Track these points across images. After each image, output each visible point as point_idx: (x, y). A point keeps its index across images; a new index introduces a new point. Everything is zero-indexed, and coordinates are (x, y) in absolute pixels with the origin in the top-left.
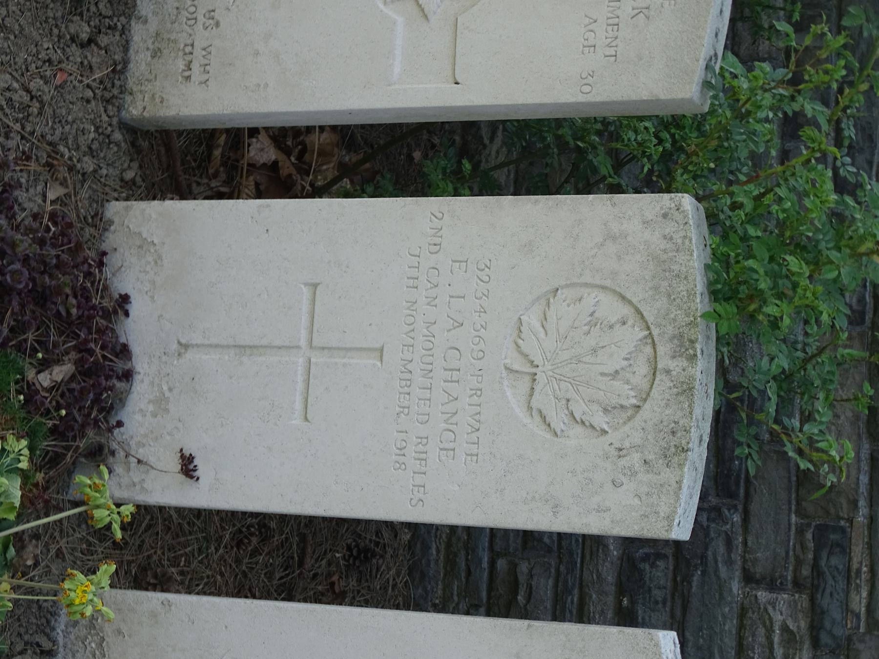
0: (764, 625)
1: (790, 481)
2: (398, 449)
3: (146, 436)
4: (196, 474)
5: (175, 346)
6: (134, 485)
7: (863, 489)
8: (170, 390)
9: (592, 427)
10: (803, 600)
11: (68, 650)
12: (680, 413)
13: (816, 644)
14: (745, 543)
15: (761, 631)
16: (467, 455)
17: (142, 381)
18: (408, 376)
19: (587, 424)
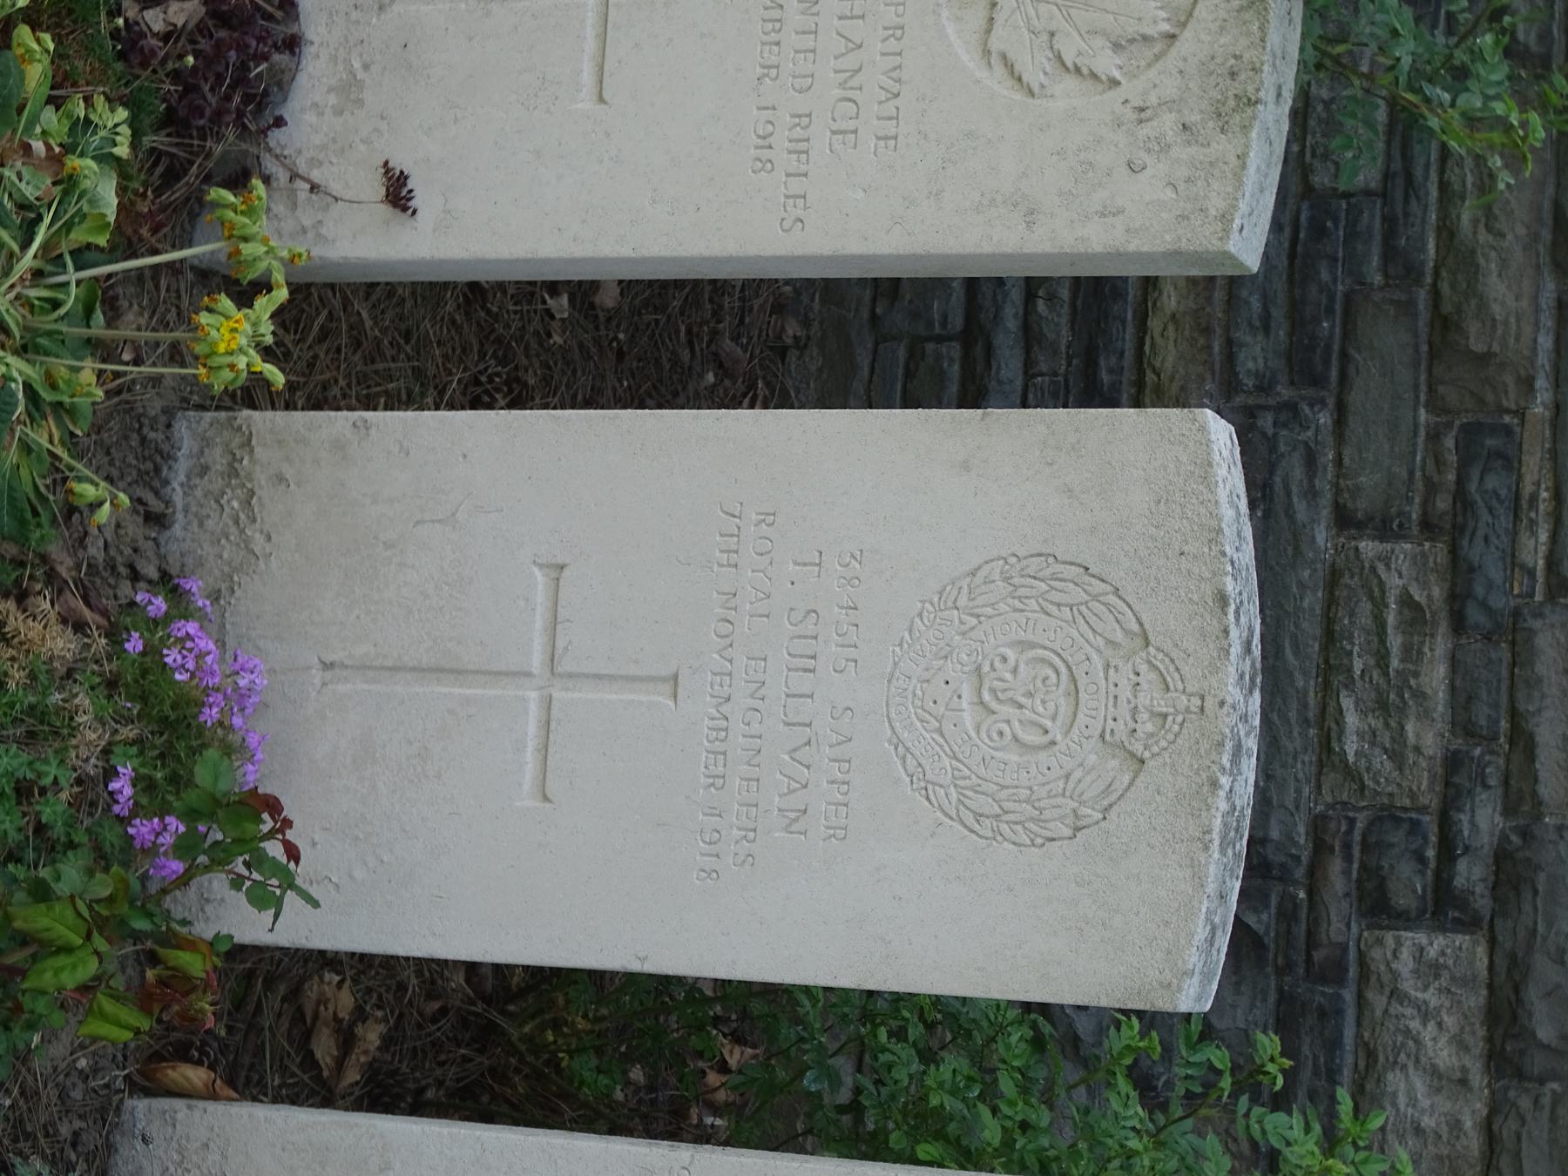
0: (1371, 598)
1: (1417, 351)
2: (759, 137)
3: (324, 147)
4: (412, 203)
6: (304, 231)
7: (1544, 359)
8: (366, 67)
9: (1094, 76)
10: (1438, 552)
11: (190, 516)
12: (1244, 42)
13: (1458, 624)
14: (1339, 462)
15: (1365, 607)
16: (878, 138)
17: (318, 56)
18: (776, 14)
19: (1085, 71)
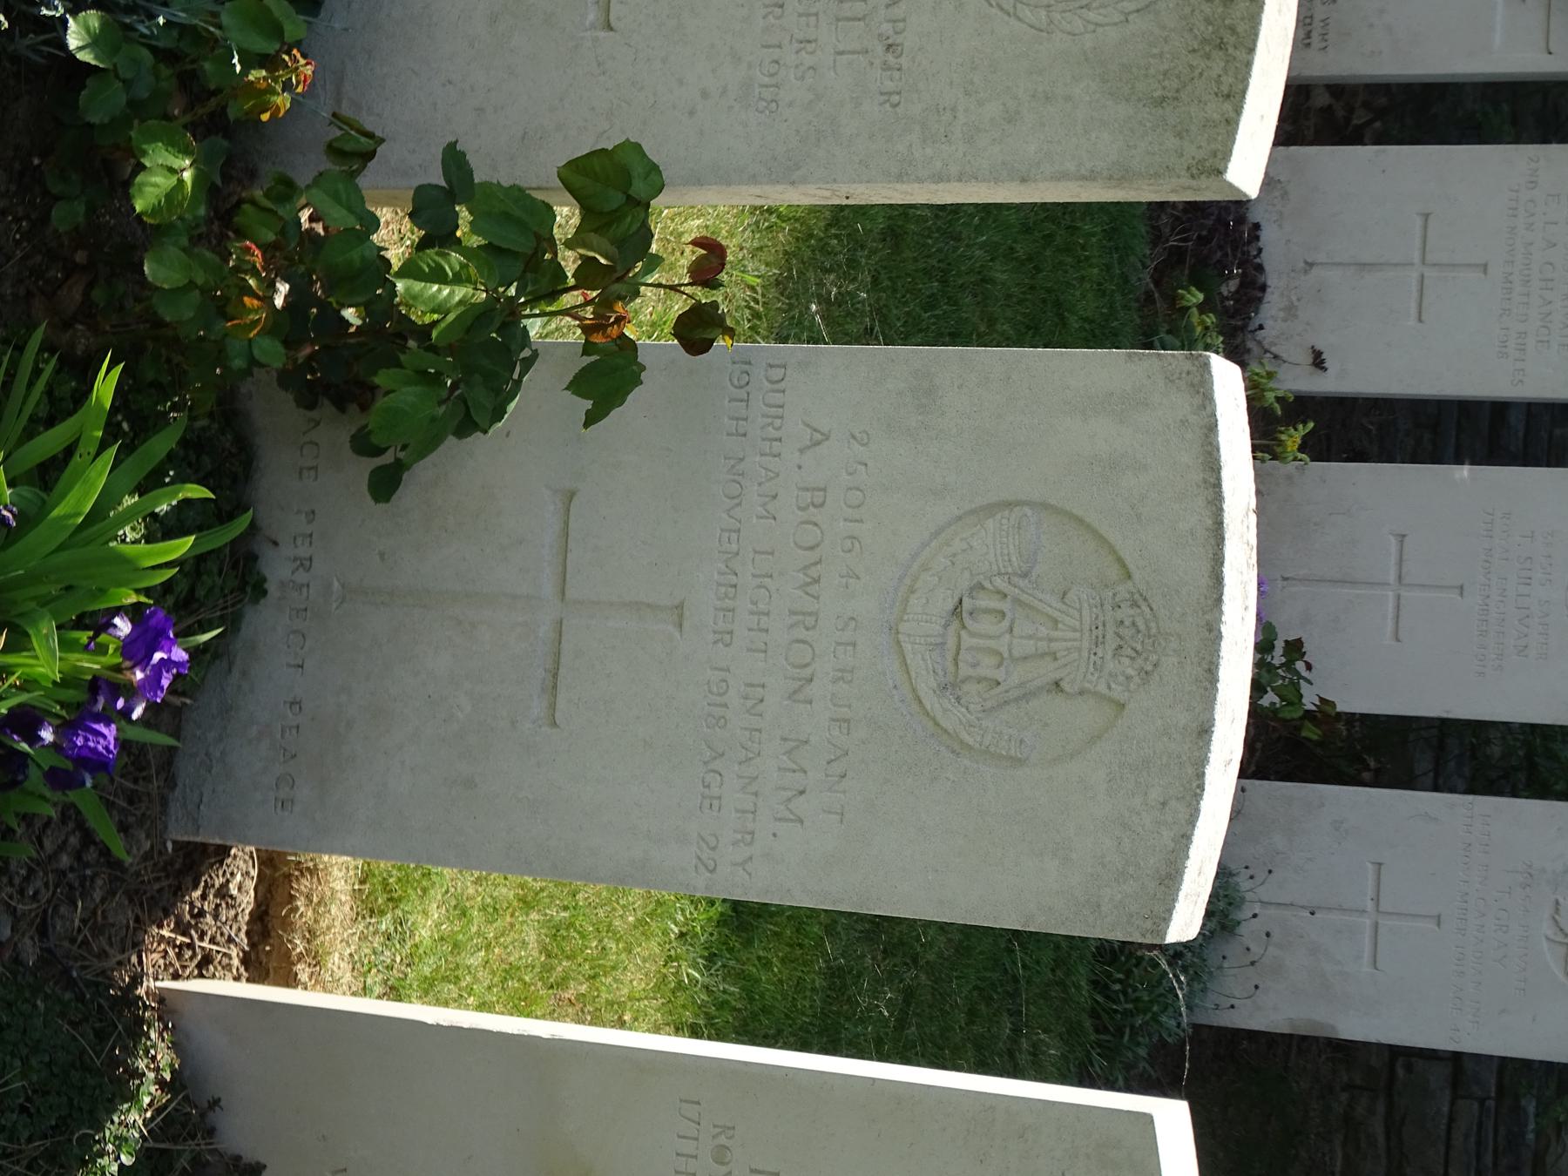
5: (1302, 265)
